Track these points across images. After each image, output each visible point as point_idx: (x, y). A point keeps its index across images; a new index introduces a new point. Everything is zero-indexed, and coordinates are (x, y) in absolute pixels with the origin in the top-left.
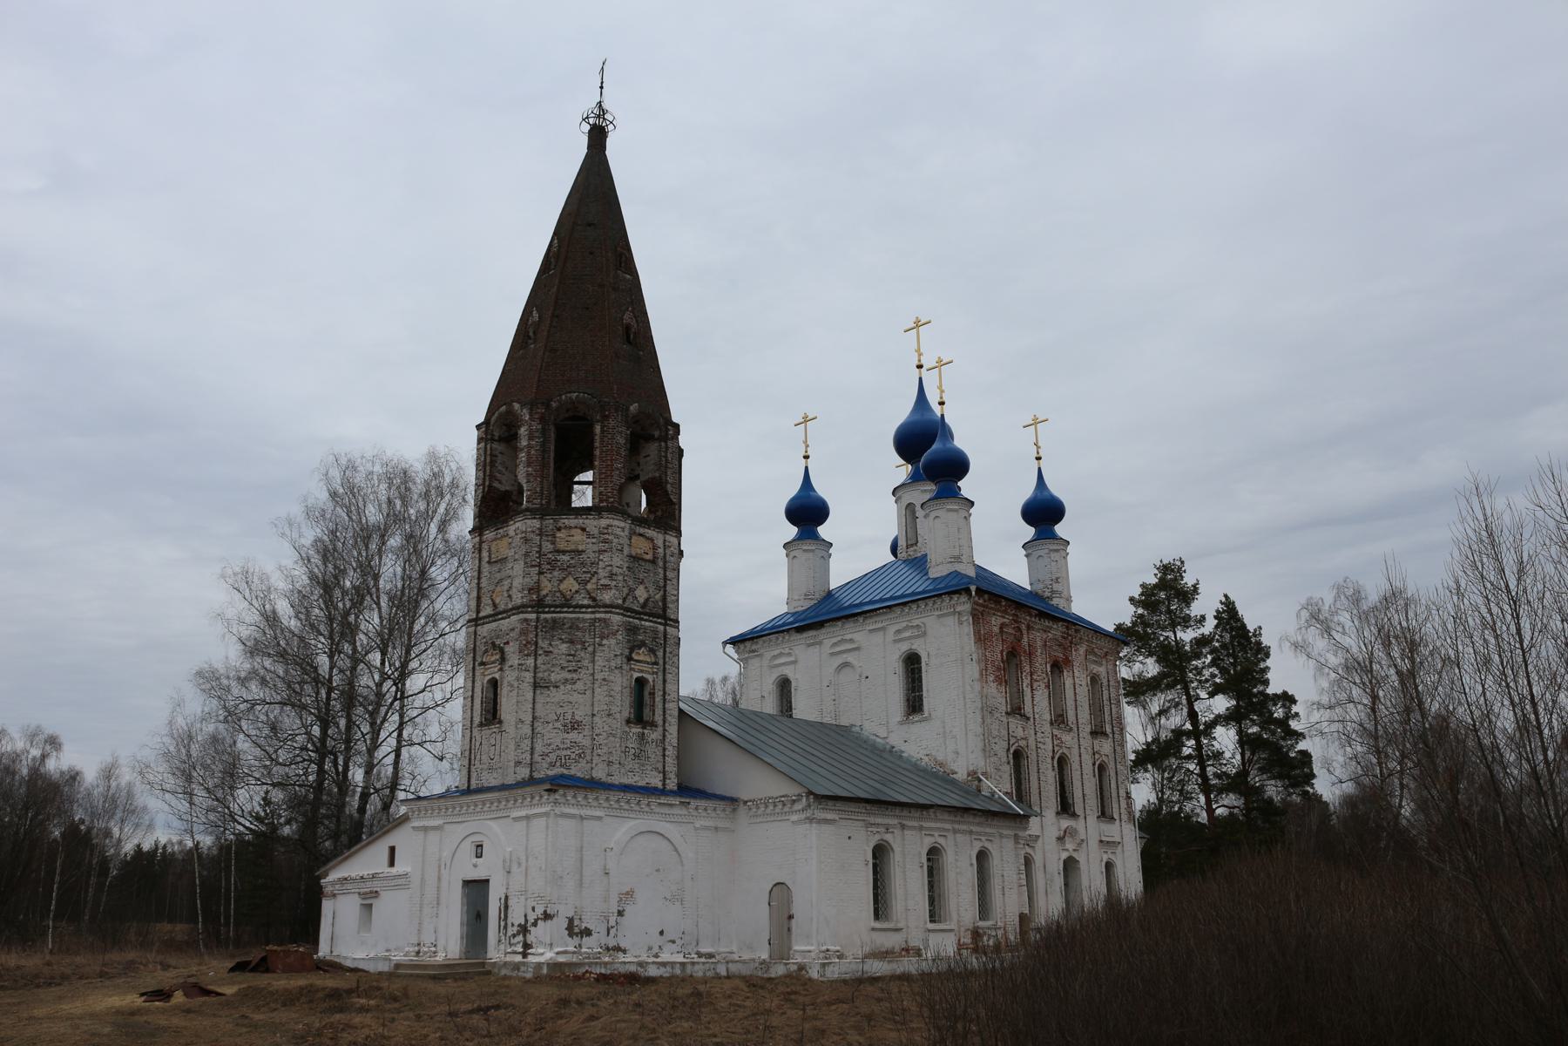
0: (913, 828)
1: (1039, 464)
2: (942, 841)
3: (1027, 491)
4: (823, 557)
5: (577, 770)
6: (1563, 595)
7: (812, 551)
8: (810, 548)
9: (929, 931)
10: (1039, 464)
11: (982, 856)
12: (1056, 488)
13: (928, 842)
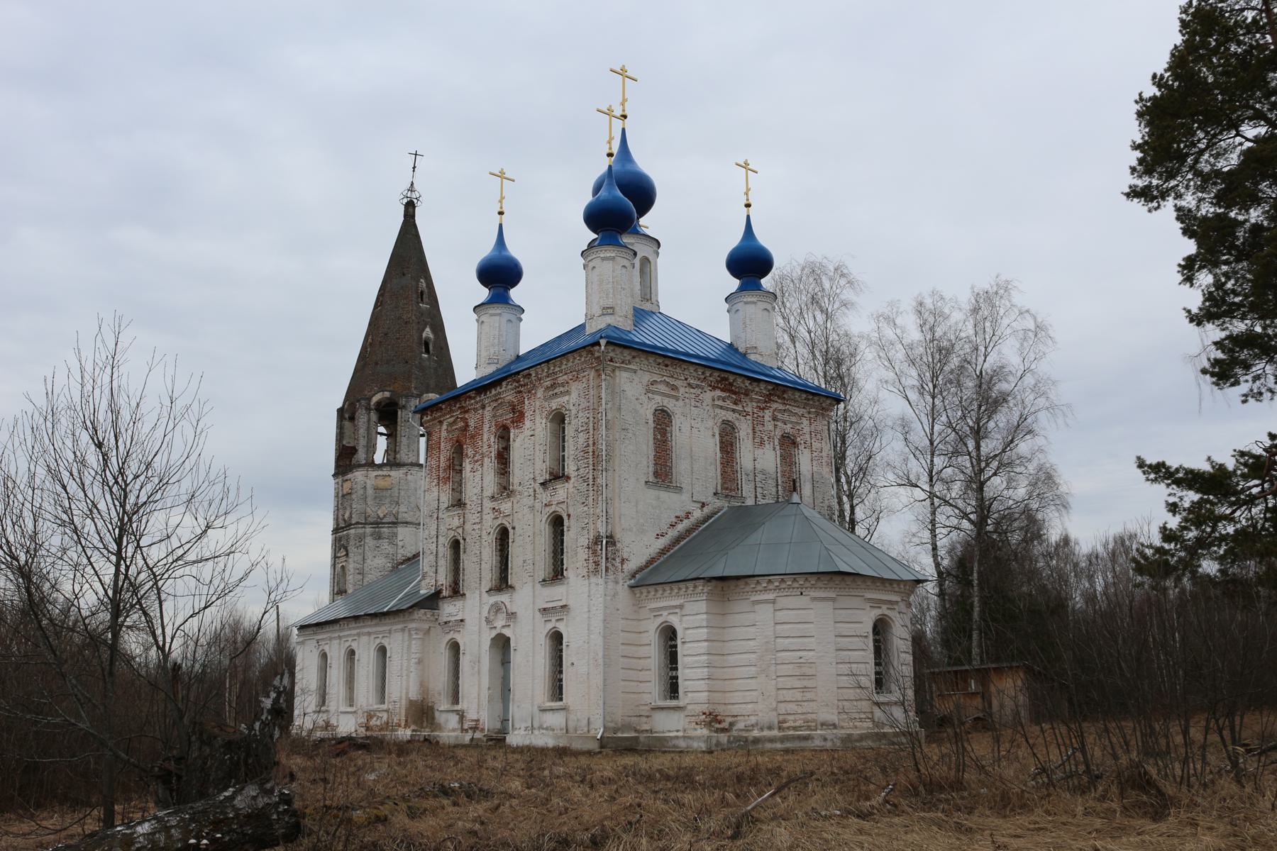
3: (485, 249)
12: (515, 249)
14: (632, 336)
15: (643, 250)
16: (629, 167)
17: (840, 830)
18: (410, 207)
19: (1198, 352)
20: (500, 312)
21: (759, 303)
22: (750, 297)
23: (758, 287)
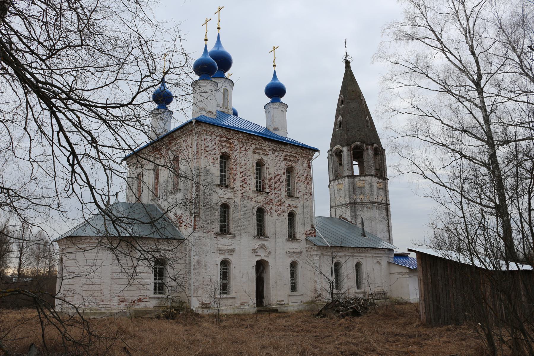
0: (369, 257)
1: (275, 68)
2: (361, 260)
3: (268, 80)
4: (282, 111)
5: (55, 190)
6: (19, 116)
7: (278, 108)
8: (276, 106)
9: (290, 296)
10: (275, 68)
11: (358, 266)
12: (282, 80)
13: (356, 261)
14: (218, 121)
15: (226, 85)
16: (220, 49)
17: (462, 337)
18: (347, 63)
19: (137, 143)
20: (277, 106)
21: (279, 108)
22: (276, 105)
23: (279, 101)
